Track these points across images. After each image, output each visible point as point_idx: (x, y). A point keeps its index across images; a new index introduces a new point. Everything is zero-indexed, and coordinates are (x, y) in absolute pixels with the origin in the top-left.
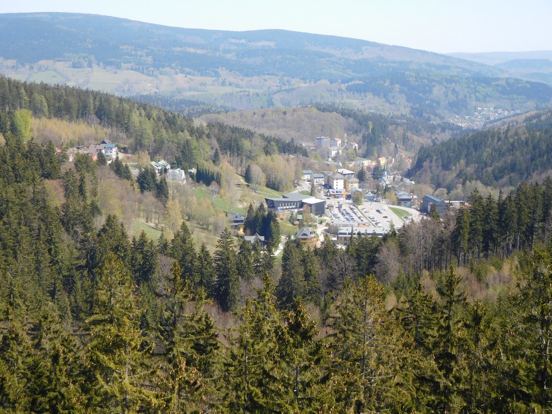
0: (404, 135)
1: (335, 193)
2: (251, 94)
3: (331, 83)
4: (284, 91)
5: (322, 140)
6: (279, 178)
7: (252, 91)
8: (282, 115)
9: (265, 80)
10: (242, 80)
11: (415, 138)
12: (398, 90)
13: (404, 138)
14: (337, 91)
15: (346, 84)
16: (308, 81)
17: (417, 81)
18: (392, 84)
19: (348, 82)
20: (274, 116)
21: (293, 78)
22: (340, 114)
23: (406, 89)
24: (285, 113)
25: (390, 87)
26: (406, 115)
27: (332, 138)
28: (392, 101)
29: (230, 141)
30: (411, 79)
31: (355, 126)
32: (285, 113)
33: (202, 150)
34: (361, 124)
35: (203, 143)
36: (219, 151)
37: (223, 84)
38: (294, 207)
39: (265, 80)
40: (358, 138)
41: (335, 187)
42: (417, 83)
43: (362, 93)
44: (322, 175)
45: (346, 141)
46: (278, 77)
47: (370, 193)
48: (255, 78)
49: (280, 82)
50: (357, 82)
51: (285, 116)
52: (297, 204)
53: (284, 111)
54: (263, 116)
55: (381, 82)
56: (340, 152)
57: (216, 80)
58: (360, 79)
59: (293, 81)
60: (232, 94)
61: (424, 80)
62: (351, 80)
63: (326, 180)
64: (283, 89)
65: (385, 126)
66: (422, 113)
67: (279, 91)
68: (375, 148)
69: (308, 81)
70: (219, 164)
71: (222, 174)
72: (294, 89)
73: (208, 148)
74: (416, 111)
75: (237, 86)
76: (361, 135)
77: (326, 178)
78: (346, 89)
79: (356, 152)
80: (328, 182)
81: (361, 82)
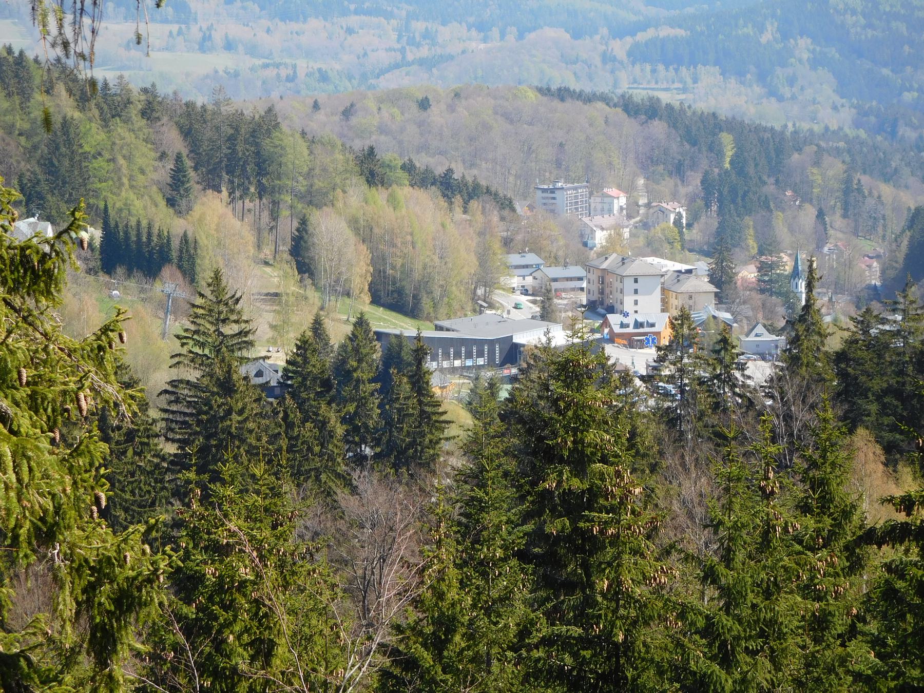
0: (848, 181)
1: (631, 330)
2: (301, 74)
3: (577, 35)
4: (413, 63)
5: (558, 194)
6: (418, 266)
7: (303, 65)
8: (414, 108)
9: (350, 31)
10: (268, 31)
11: (886, 190)
12: (805, 56)
13: (847, 192)
14: (598, 61)
15: (629, 40)
16: (495, 32)
17: (870, 26)
18: (785, 36)
19: (633, 34)
20: (385, 114)
21: (444, 24)
22: (619, 110)
23: (833, 52)
24: (424, 104)
25: (779, 46)
26: (841, 129)
27: (595, 188)
28: (786, 92)
29: (231, 139)
30: (850, 19)
31: (674, 147)
32: (424, 104)
33: (121, 161)
34: (694, 143)
35: (127, 135)
36: (188, 163)
37: (205, 44)
38: (481, 361)
39: (350, 31)
40: (683, 190)
41: (628, 306)
42: (870, 33)
43: (683, 70)
44: (578, 271)
45: (643, 201)
46: (394, 22)
47: (760, 329)
48: (315, 23)
49: (400, 37)
50: (665, 32)
51: (425, 114)
52: (492, 353)
53: (420, 97)
54: (347, 113)
55: (749, 30)
56: (626, 233)
57: (180, 33)
58: (673, 23)
59: (445, 33)
60: (236, 75)
61: (894, 24)
62: (644, 27)
63: (595, 287)
64: (410, 57)
65: (779, 151)
66: (894, 125)
67: (397, 66)
68: (749, 221)
69: (495, 32)
70: (189, 209)
71: (203, 241)
72: (451, 58)
73: (145, 156)
74: (873, 119)
75: (252, 50)
76: (695, 181)
77: (594, 277)
78: (630, 54)
79: (681, 233)
80: (602, 292)
81: (680, 32)
